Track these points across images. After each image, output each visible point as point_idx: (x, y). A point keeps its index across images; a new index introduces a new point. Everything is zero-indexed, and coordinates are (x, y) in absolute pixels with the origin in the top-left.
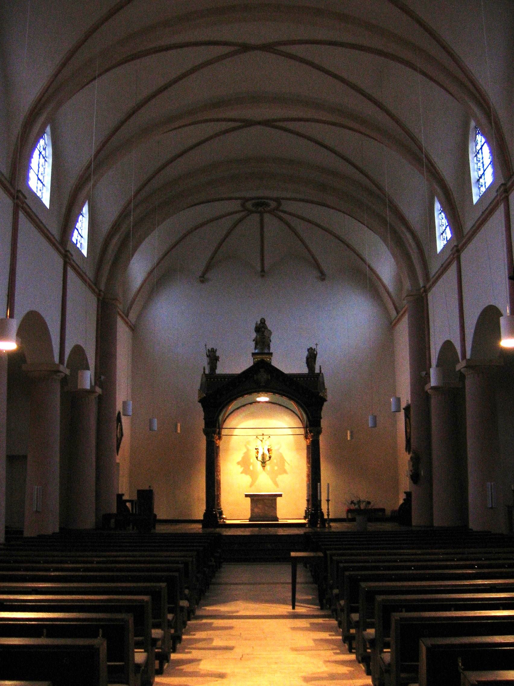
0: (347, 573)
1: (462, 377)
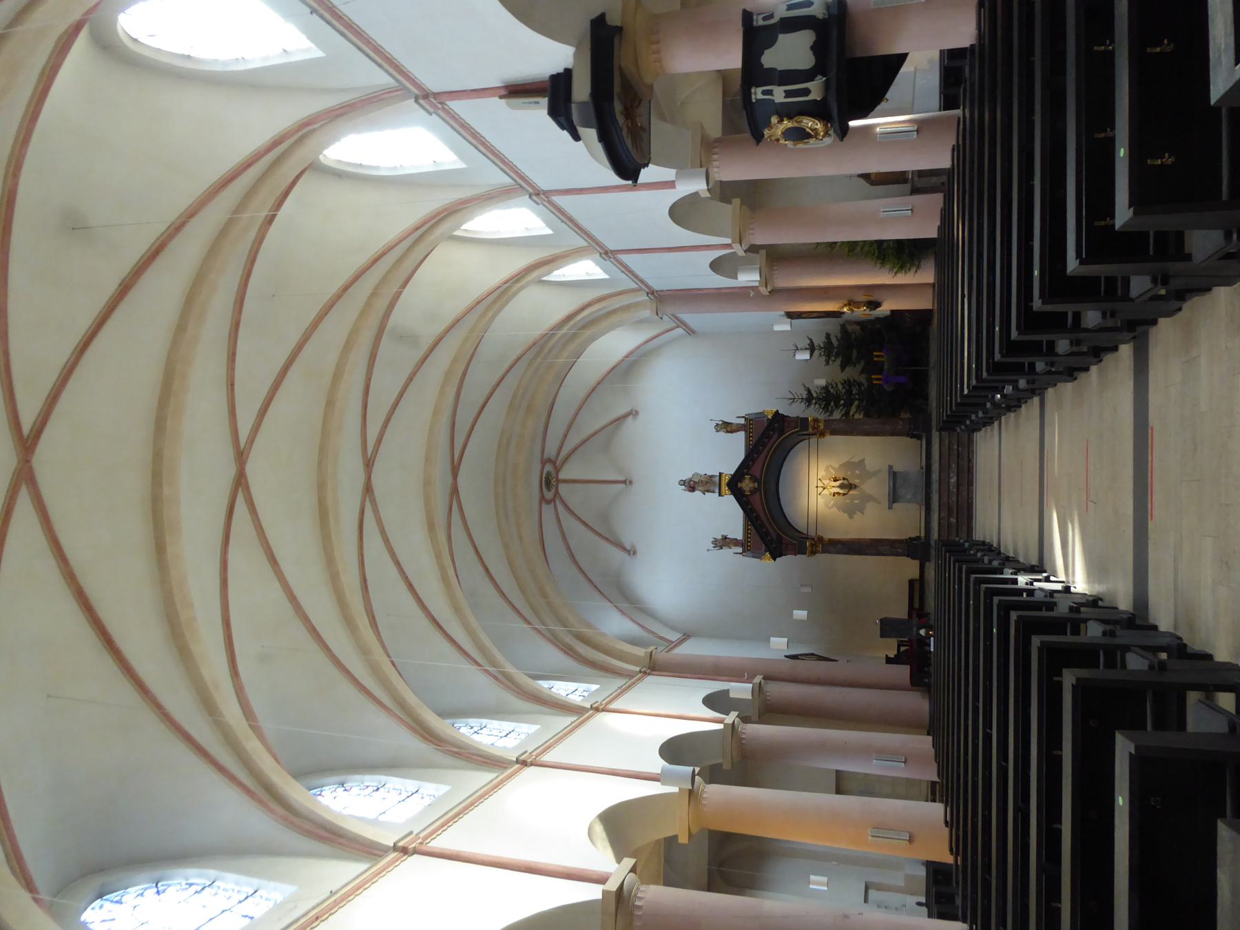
0: (985, 375)
1: (753, 249)
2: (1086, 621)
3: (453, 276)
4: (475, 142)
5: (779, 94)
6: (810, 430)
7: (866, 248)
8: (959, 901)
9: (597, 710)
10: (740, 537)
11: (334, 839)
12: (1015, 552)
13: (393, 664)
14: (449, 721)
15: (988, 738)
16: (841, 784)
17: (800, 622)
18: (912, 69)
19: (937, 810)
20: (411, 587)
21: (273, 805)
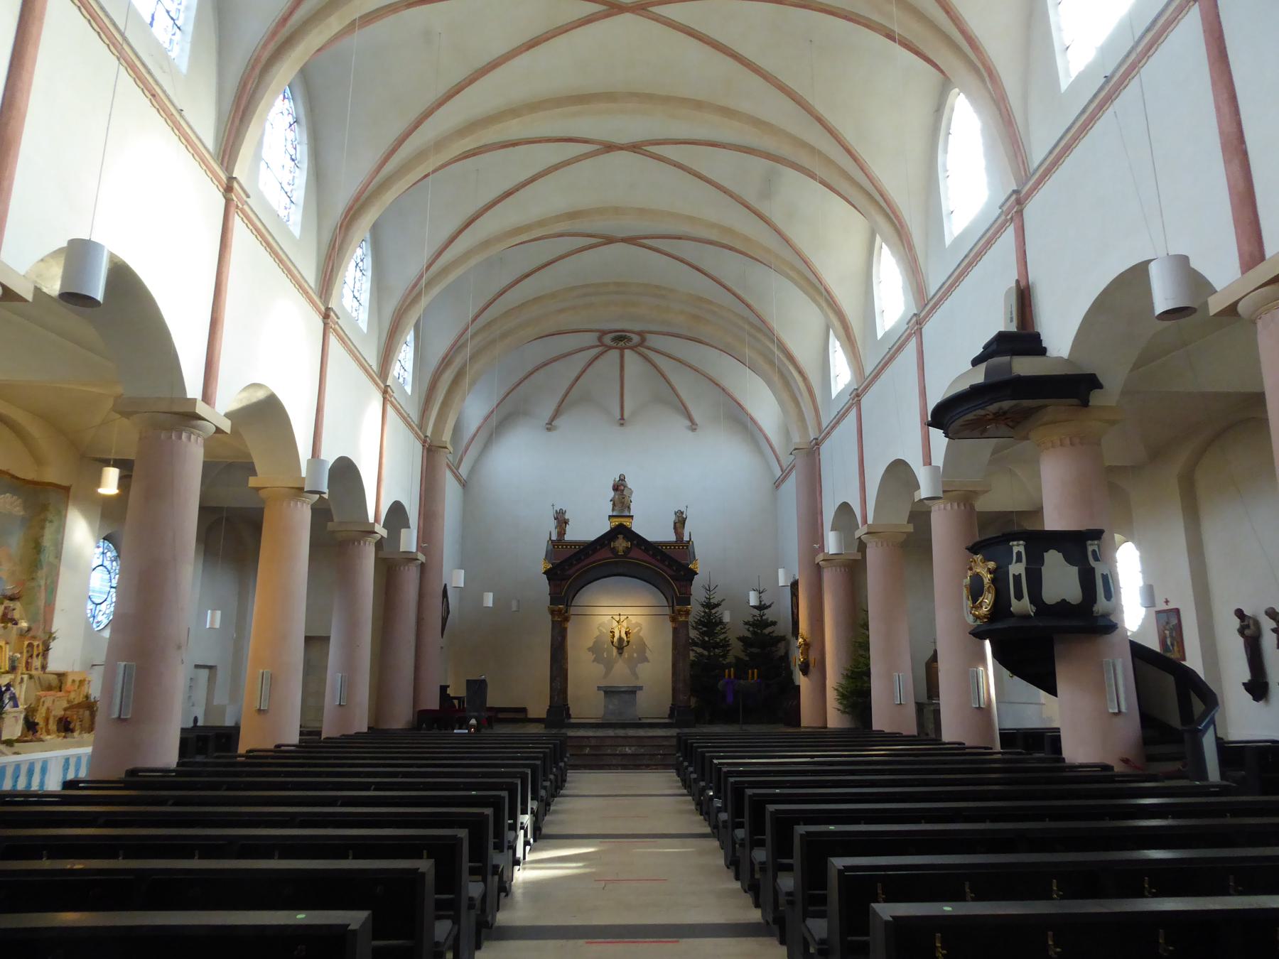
0: (732, 780)
1: (862, 547)
2: (484, 880)
3: (833, 234)
4: (972, 255)
5: (1017, 569)
6: (677, 607)
7: (862, 660)
8: (199, 759)
9: (385, 392)
10: (568, 537)
11: (238, 114)
12: (556, 812)
13: (426, 176)
14: (368, 236)
15: (366, 787)
16: (316, 643)
17: (481, 599)
18: (1043, 701)
19: (292, 737)
20: (508, 194)
21: (272, 47)
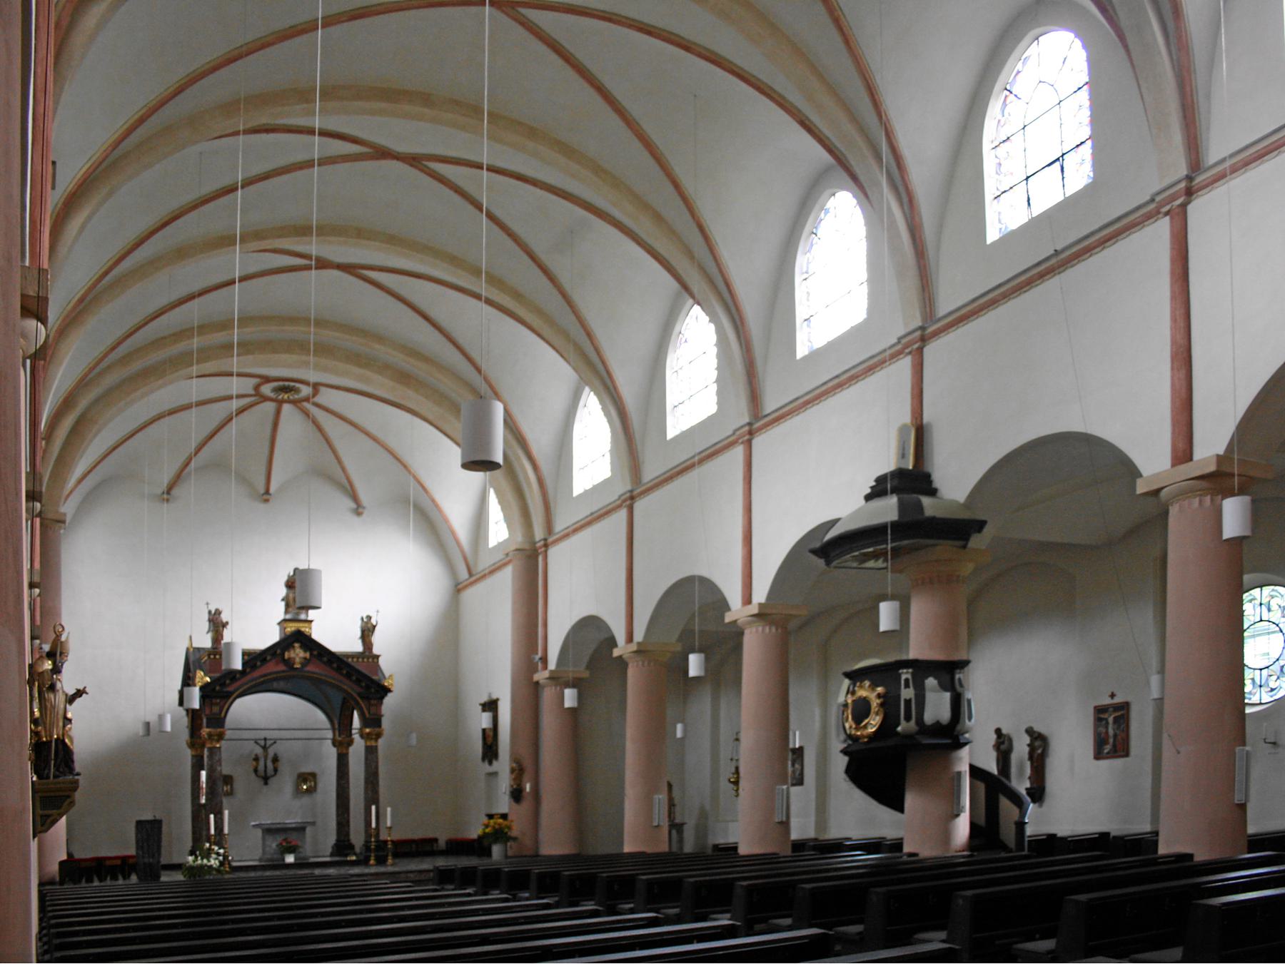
4: (845, 376)
